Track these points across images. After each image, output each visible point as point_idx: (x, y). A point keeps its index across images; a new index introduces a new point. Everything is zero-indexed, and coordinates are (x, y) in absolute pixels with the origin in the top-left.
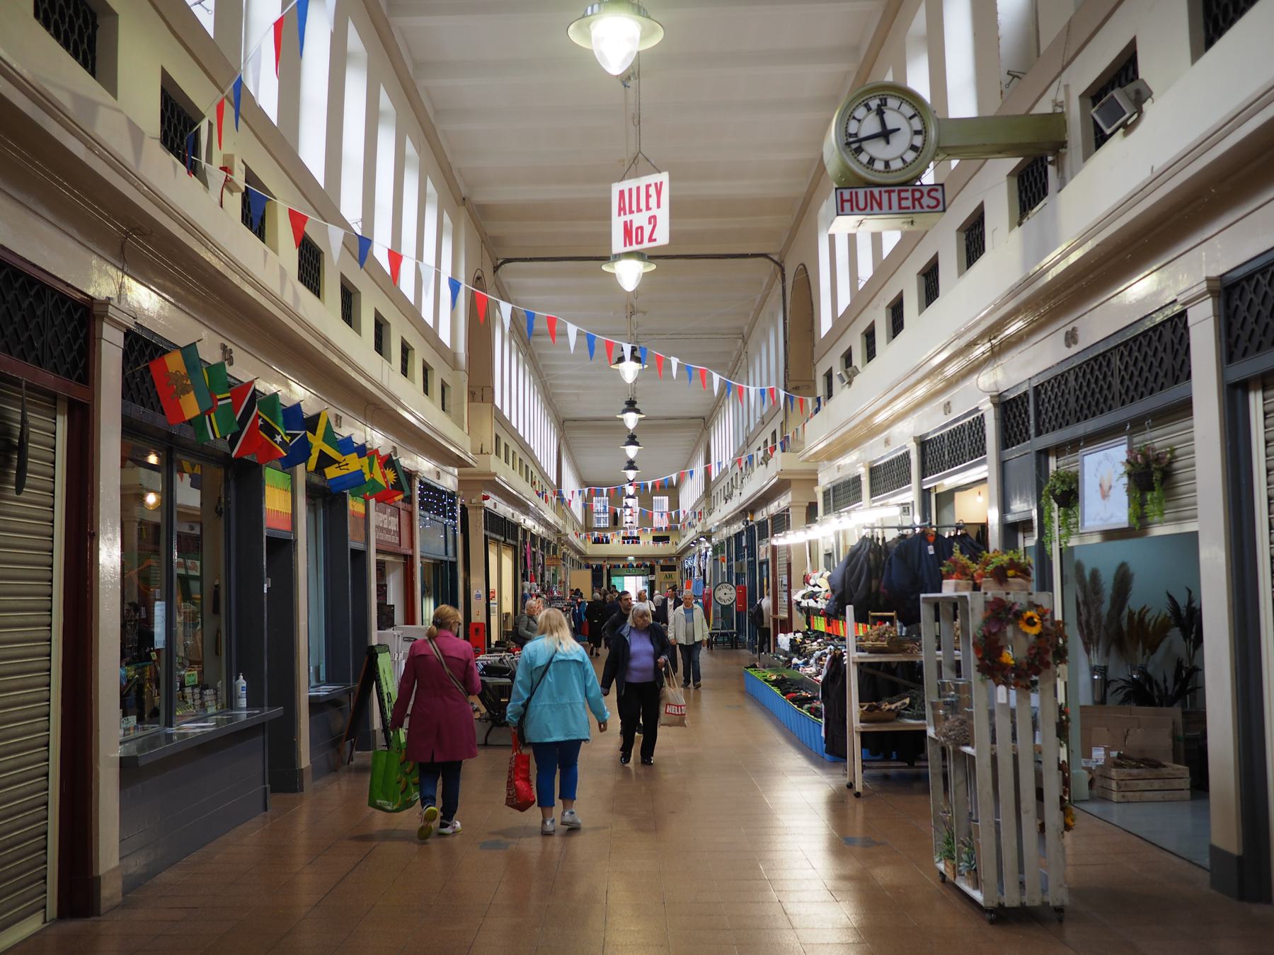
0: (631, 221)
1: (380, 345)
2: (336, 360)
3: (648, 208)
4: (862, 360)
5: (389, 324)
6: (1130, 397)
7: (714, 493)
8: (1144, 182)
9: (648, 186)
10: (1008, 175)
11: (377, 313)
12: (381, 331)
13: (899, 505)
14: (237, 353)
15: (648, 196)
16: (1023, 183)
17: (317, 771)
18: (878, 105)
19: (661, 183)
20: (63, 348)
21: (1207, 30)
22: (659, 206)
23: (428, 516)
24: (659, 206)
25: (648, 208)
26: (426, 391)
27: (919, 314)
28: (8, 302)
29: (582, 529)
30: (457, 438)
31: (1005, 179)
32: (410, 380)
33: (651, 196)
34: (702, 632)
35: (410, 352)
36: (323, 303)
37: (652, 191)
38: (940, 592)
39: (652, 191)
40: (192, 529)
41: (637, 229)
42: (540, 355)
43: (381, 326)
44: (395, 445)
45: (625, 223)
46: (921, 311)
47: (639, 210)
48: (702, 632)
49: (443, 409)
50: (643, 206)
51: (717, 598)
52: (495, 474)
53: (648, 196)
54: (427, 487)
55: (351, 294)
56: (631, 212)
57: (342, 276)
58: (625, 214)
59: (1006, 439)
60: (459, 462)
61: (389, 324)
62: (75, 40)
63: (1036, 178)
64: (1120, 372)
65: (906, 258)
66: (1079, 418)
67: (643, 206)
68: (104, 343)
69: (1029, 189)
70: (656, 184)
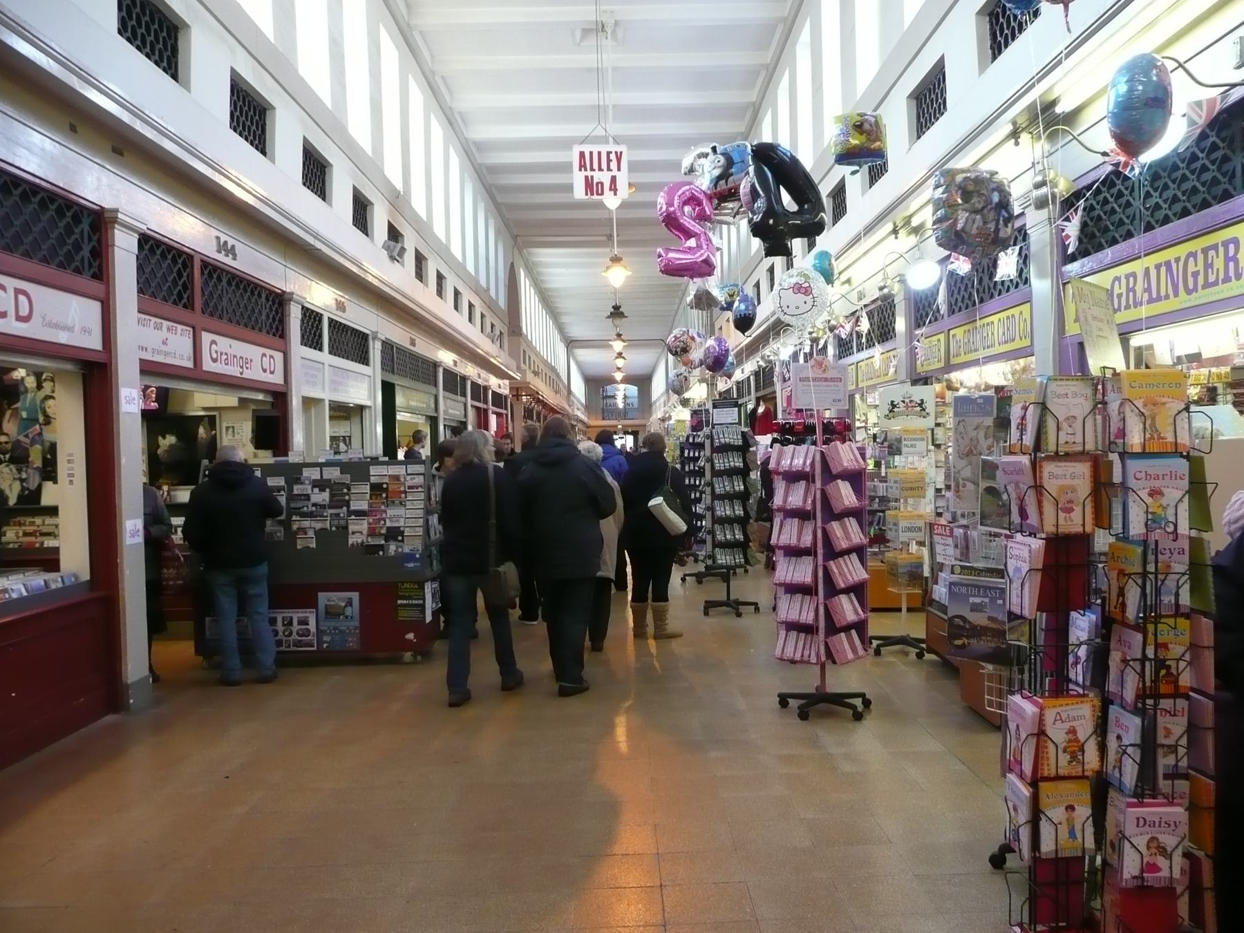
0: (592, 177)
1: (420, 275)
2: (472, 346)
3: (609, 169)
4: (782, 268)
5: (331, 166)
6: (1006, 287)
7: (717, 327)
9: (609, 153)
10: (977, 13)
11: (470, 302)
14: (418, 341)
15: (609, 161)
16: (921, 106)
19: (621, 153)
21: (918, 131)
22: (619, 169)
23: (448, 394)
24: (619, 169)
25: (609, 169)
26: (470, 320)
27: (980, 75)
30: (498, 356)
31: (765, 272)
32: (328, 204)
35: (400, 238)
36: (273, 161)
37: (613, 156)
38: (286, 455)
39: (613, 156)
42: (545, 289)
43: (420, 259)
45: (586, 177)
47: (600, 169)
49: (482, 332)
50: (604, 166)
52: (529, 383)
53: (609, 161)
54: (447, 372)
55: (265, 110)
56: (592, 169)
57: (455, 288)
59: (917, 319)
60: (510, 378)
61: (274, 108)
62: (146, 22)
63: (937, 94)
64: (988, 270)
65: (752, 273)
66: (992, 293)
67: (604, 166)
69: (939, 95)
70: (616, 153)
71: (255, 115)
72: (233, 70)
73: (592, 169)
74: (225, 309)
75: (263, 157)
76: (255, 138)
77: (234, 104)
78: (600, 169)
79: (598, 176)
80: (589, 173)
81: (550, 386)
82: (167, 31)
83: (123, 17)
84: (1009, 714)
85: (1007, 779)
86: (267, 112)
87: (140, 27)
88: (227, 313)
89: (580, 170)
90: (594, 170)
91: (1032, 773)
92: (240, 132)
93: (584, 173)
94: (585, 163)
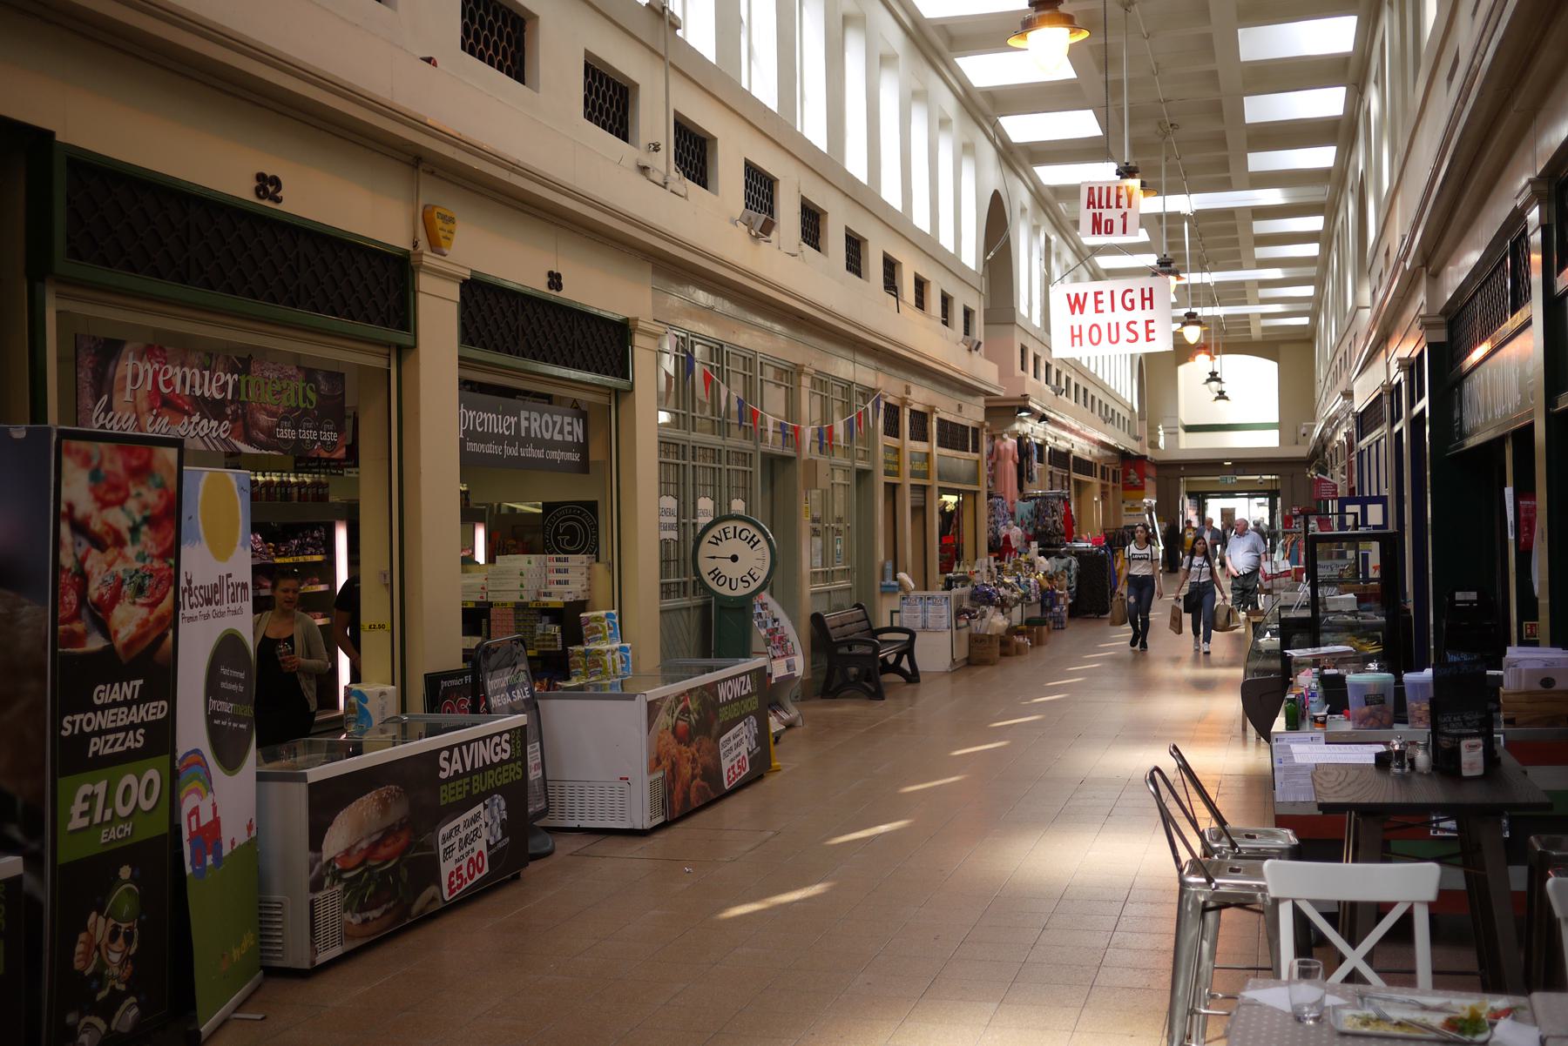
0: (1100, 214)
3: (1118, 206)
8: (541, 171)
12: (968, 317)
13: (310, 374)
15: (1118, 197)
17: (254, 483)
18: (280, 189)
20: (513, 308)
25: (1118, 206)
28: (323, 284)
29: (812, 465)
32: (865, 279)
33: (1121, 197)
34: (227, 422)
40: (1227, 515)
41: (1106, 222)
43: (855, 245)
44: (909, 396)
45: (1094, 215)
46: (916, 273)
47: (1109, 206)
48: (227, 422)
50: (1113, 202)
51: (763, 544)
53: (1118, 197)
56: (1101, 207)
58: (1094, 207)
67: (1113, 202)
68: (421, 298)
71: (609, 90)
72: (916, 273)
73: (1101, 207)
74: (520, 328)
75: (855, 277)
76: (497, 53)
77: (588, 88)
78: (1109, 206)
79: (1107, 214)
80: (1097, 211)
81: (1118, 426)
82: (503, 20)
83: (466, 23)
84: (1489, 1032)
85: (587, 598)
86: (707, 143)
87: (483, 28)
88: (524, 334)
89: (1088, 207)
90: (1103, 207)
91: (324, 963)
92: (604, 122)
93: (1092, 210)
94: (1094, 200)
